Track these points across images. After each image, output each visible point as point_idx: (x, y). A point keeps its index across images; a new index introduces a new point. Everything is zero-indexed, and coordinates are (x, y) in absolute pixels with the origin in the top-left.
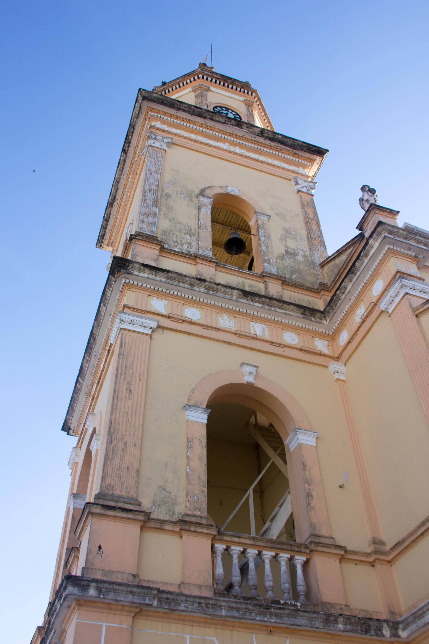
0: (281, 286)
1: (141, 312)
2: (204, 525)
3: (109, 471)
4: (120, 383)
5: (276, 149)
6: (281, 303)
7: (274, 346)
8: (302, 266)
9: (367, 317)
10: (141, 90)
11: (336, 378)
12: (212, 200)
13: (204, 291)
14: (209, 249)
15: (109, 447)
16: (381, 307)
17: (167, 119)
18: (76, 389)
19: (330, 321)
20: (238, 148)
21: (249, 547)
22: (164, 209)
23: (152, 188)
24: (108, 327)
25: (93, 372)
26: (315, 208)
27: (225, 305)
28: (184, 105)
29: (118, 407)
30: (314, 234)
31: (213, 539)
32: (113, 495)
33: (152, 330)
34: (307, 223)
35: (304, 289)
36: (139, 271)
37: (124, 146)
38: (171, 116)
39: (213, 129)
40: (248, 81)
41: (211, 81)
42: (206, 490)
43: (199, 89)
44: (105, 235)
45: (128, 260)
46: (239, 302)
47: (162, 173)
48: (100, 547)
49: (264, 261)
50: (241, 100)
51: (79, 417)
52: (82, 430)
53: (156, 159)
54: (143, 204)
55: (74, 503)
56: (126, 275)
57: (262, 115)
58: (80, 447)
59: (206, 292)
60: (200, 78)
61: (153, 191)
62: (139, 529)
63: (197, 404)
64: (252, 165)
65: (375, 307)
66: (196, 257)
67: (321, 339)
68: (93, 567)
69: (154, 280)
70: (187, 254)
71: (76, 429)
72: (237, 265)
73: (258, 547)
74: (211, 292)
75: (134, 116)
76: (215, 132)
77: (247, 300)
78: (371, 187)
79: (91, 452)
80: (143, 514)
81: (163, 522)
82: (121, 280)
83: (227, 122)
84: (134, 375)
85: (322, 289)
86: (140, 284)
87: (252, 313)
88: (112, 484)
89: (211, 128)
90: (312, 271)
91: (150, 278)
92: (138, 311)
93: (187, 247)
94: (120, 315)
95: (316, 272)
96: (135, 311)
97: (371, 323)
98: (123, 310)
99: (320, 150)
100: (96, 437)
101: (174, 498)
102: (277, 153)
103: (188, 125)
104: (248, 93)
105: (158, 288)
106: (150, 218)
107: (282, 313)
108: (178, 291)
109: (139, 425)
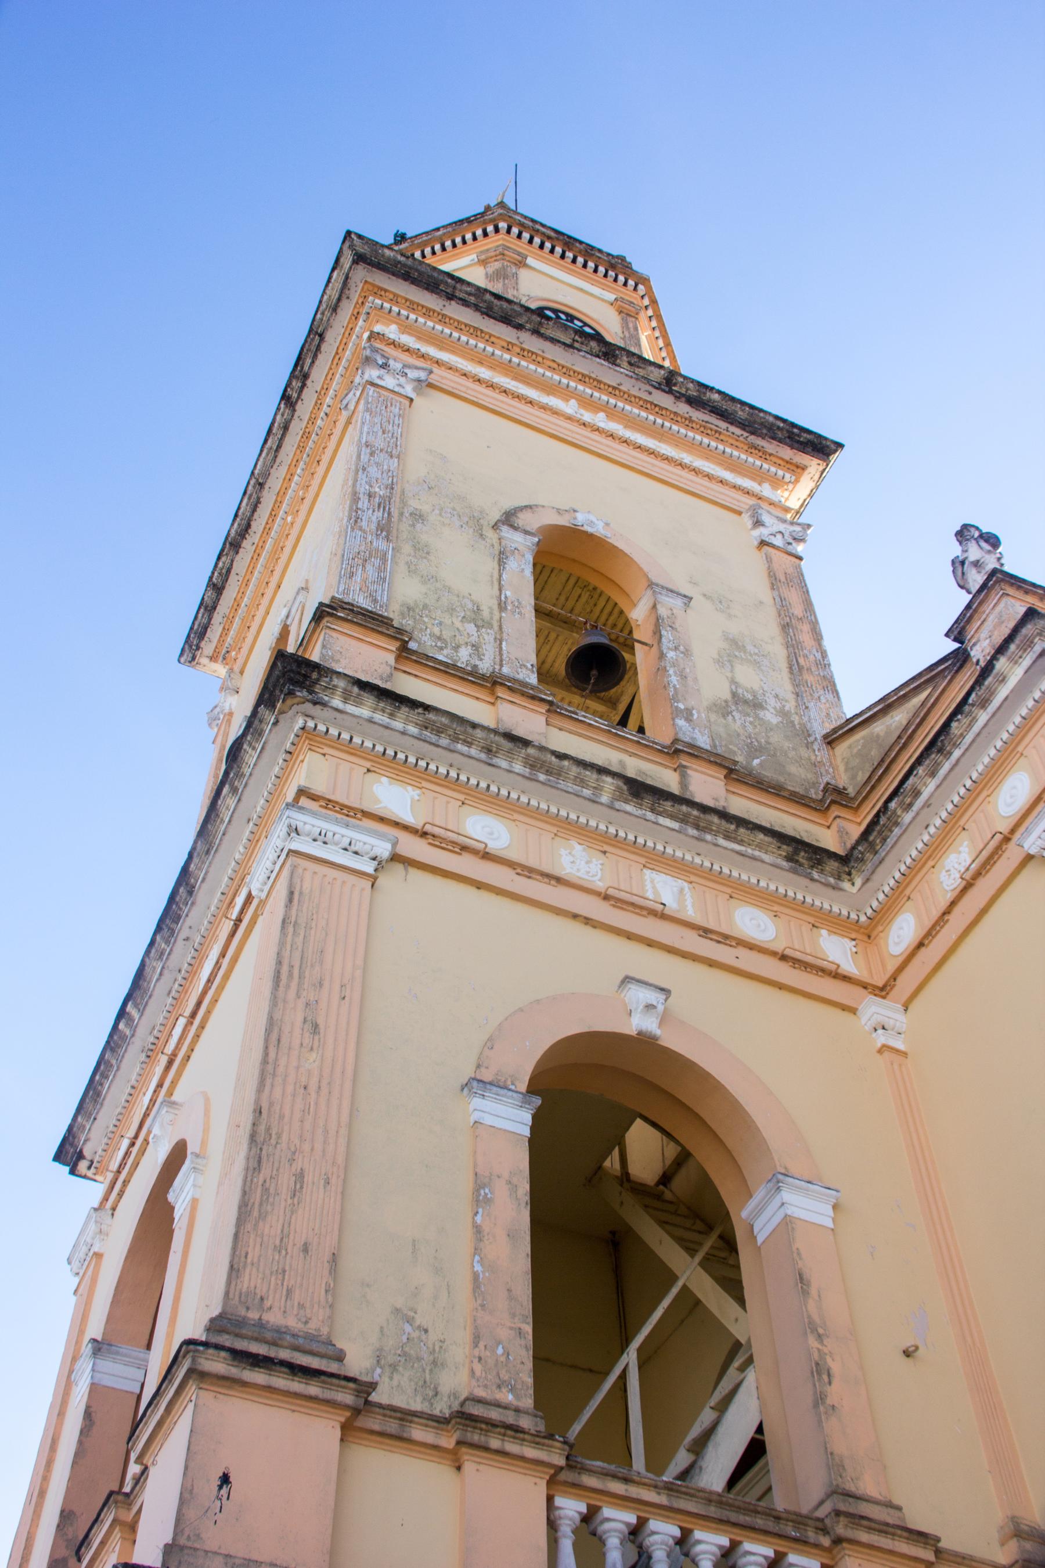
0: (723, 783)
1: (345, 811)
2: (528, 1433)
3: (250, 1250)
4: (285, 1001)
5: (704, 429)
6: (731, 823)
7: (711, 939)
8: (776, 738)
9: (978, 874)
10: (353, 236)
11: (879, 1045)
12: (537, 539)
13: (521, 772)
14: (529, 666)
15: (252, 1181)
16: (1026, 846)
17: (416, 321)
18: (115, 1038)
19: (864, 884)
20: (602, 415)
21: (654, 1514)
22: (407, 549)
23: (376, 492)
24: (237, 856)
25: (176, 986)
26: (808, 592)
27: (578, 817)
28: (465, 288)
29: (281, 1070)
30: (805, 656)
31: (551, 1482)
32: (260, 1324)
33: (376, 863)
34: (785, 627)
35: (784, 797)
36: (345, 700)
37: (288, 385)
38: (428, 313)
39: (540, 359)
40: (624, 255)
41: (531, 241)
42: (528, 1329)
43: (498, 258)
44: (209, 629)
45: (316, 666)
46: (618, 810)
47: (402, 456)
48: (225, 1479)
49: (677, 713)
50: (606, 298)
51: (114, 1122)
52: (124, 1158)
53: (385, 420)
54: (353, 529)
55: (93, 1370)
56: (308, 707)
57: (657, 345)
58: (114, 1209)
59: (527, 775)
60: (501, 231)
61: (377, 500)
62: (338, 1433)
63: (503, 1080)
64: (639, 463)
65: (1004, 847)
66: (495, 683)
67: (835, 933)
68: (197, 1545)
69: (387, 728)
70: (470, 674)
71: (100, 1156)
72: (605, 718)
73: (679, 1516)
74: (542, 777)
75: (324, 306)
76: (542, 367)
77: (640, 806)
78: (984, 531)
79: (173, 1208)
80: (351, 1385)
81: (406, 1416)
82: (293, 719)
83: (576, 345)
84: (326, 984)
85: (833, 802)
86: (345, 736)
87: (650, 844)
88: (258, 1291)
89: (534, 356)
90: (804, 753)
91: (376, 720)
92: (337, 809)
93: (470, 655)
94: (288, 813)
95: (813, 758)
96: (330, 809)
97: (992, 892)
98: (296, 799)
99: (820, 443)
100: (192, 1162)
101: (437, 1348)
102: (706, 441)
103: (472, 342)
104: (625, 284)
105: (396, 753)
106: (369, 567)
107: (733, 850)
108: (451, 766)
109: (339, 1126)
